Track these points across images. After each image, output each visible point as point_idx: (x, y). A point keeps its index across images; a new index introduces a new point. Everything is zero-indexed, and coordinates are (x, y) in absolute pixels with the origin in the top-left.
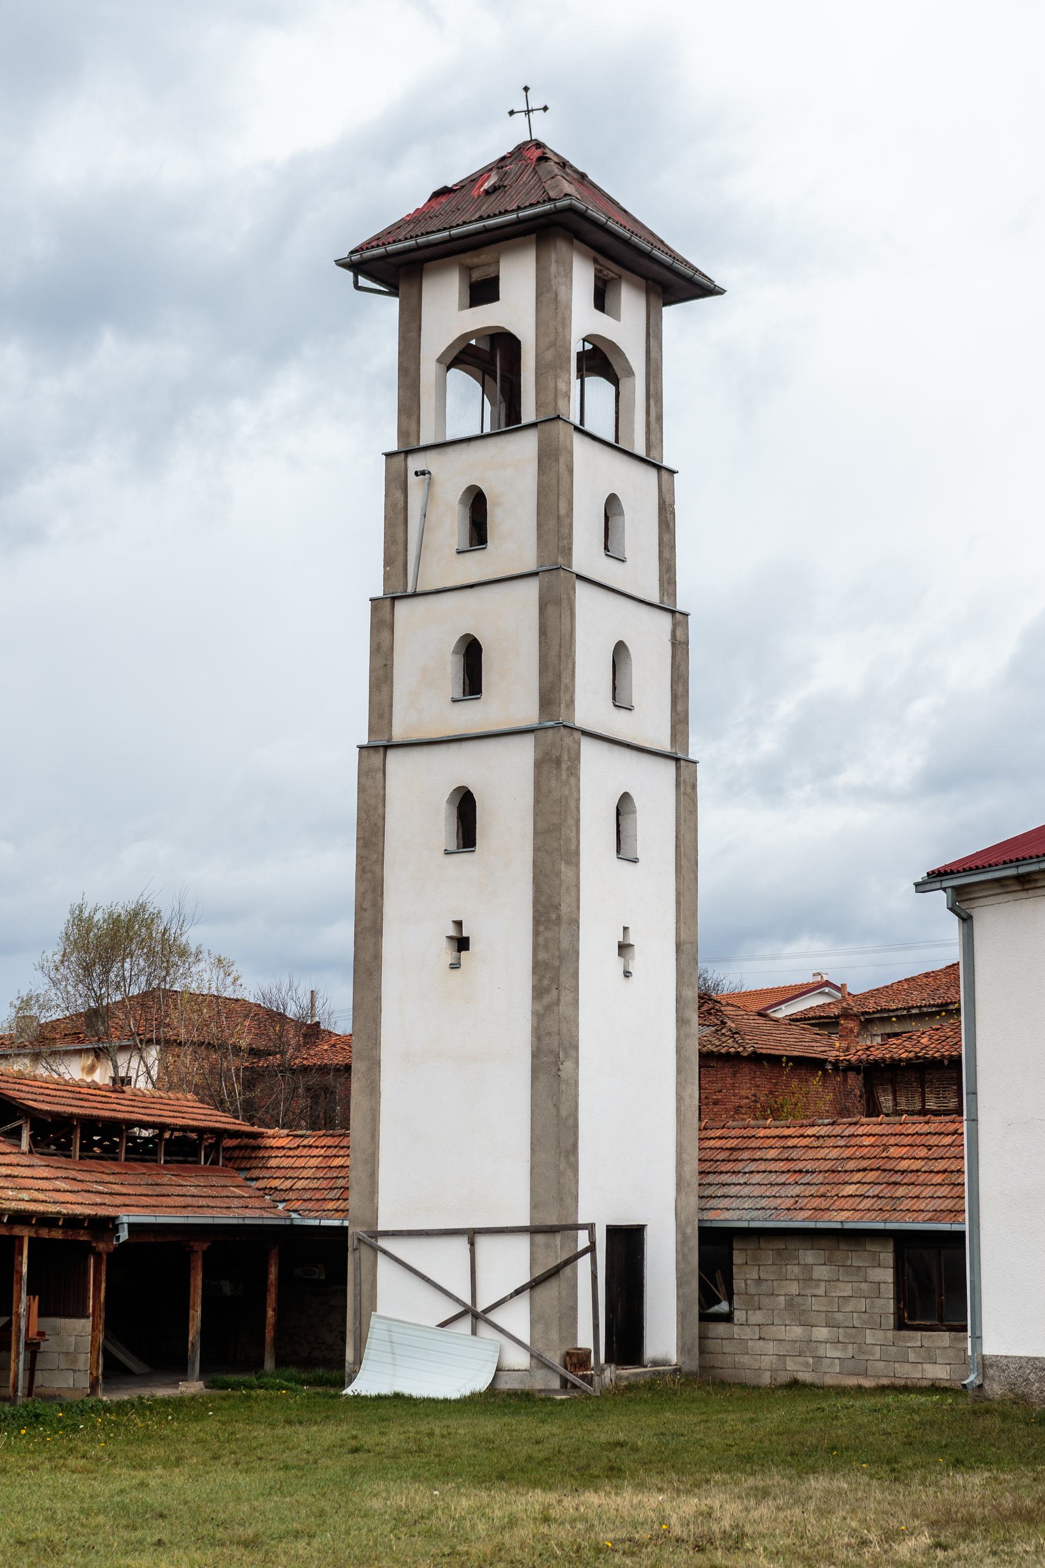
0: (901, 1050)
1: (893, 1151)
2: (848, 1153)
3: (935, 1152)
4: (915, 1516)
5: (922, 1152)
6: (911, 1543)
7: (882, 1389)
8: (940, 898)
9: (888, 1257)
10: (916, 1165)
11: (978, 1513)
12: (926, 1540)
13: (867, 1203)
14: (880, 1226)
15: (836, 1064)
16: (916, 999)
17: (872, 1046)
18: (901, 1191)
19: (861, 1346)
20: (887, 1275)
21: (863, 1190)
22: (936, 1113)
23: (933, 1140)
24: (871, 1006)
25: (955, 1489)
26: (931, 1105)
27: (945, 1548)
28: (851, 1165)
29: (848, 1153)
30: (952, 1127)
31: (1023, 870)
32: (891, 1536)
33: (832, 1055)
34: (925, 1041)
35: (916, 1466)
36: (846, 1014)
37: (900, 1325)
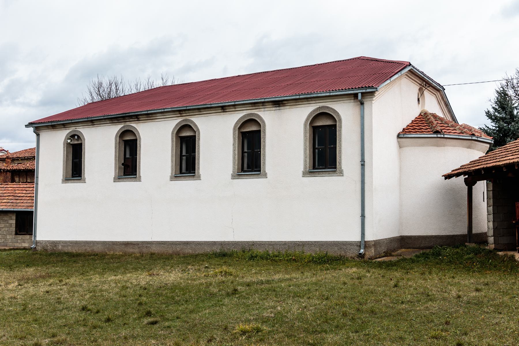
0: (21, 167)
1: (17, 192)
2: (4, 192)
3: (28, 192)
4: (14, 278)
5: (25, 192)
6: (12, 285)
7: (11, 249)
8: (31, 129)
9: (14, 217)
10: (22, 195)
11: (30, 277)
12: (16, 284)
13: (9, 204)
14: (12, 210)
15: (4, 170)
16: (27, 155)
17: (15, 166)
18: (18, 201)
19: (6, 239)
20: (14, 222)
21: (8, 201)
22: (29, 183)
23: (27, 189)
24: (15, 156)
25: (26, 272)
26: (29, 181)
27: (21, 286)
28: (5, 195)
29: (4, 192)
30: (32, 186)
31: (53, 124)
32: (7, 284)
33: (3, 168)
34: (28, 165)
35: (17, 267)
36: (8, 158)
37: (16, 234)
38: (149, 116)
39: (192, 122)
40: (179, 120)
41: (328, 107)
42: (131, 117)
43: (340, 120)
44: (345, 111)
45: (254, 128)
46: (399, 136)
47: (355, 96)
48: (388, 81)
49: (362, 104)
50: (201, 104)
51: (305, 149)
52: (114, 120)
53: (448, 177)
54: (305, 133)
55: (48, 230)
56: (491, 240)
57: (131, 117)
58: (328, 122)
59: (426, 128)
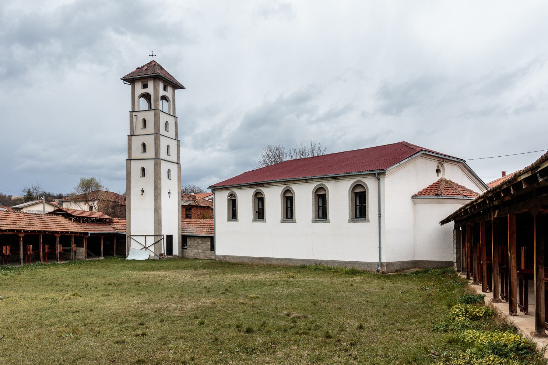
38: (269, 184)
39: (291, 188)
40: (229, 192)
41: (361, 181)
42: (260, 184)
43: (368, 189)
44: (370, 184)
45: (323, 193)
46: (413, 197)
47: (375, 174)
48: (398, 164)
49: (379, 179)
50: (294, 177)
51: (349, 206)
52: (252, 186)
53: (442, 223)
54: (349, 196)
55: (224, 248)
56: (455, 264)
57: (260, 184)
58: (362, 190)
59: (435, 192)
